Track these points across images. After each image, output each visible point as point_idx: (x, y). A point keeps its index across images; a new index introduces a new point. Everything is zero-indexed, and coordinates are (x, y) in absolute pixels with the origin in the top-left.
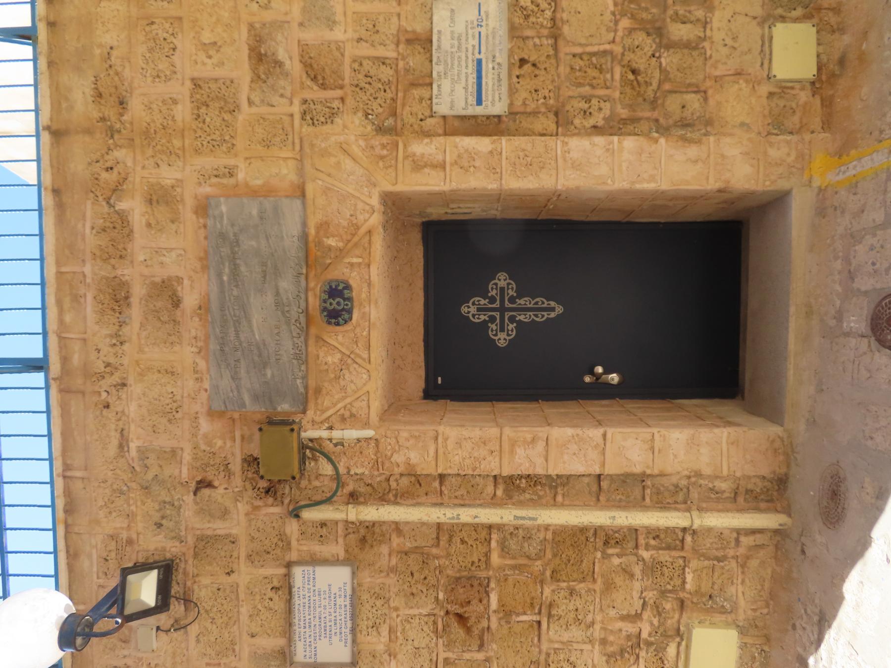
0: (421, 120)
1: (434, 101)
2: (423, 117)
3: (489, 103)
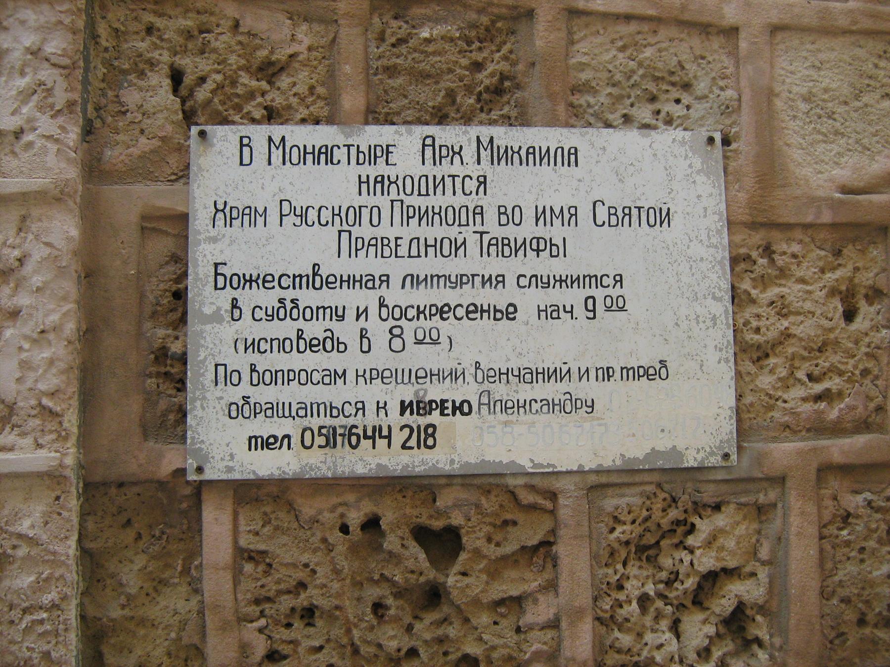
0: (176, 77)
1: (259, 134)
2: (188, 80)
3: (244, 389)
